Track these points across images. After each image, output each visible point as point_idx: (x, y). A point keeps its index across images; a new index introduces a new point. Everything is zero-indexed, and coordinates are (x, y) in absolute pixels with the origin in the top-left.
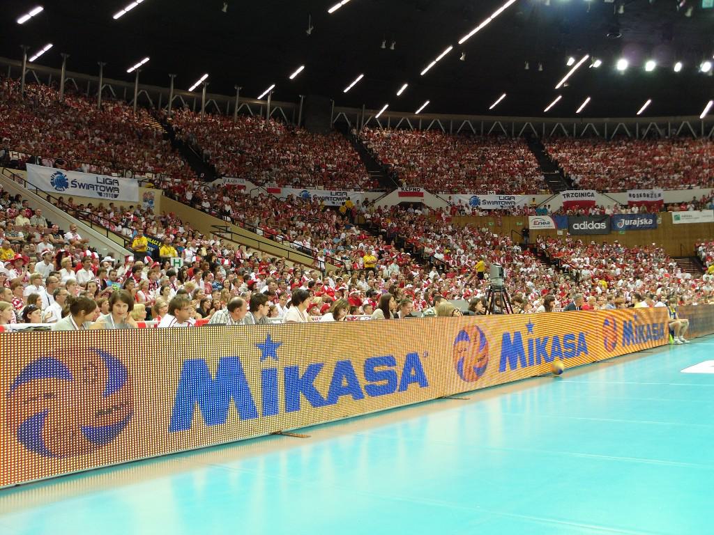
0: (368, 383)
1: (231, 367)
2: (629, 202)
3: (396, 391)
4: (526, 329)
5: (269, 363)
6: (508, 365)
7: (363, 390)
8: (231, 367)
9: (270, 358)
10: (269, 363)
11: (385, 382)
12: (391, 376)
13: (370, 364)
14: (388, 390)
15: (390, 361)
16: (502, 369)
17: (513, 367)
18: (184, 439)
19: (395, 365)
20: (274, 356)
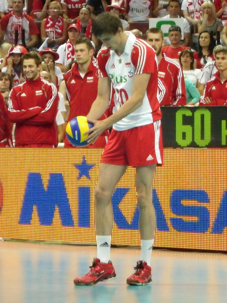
0: (174, 216)
1: (57, 180)
2: (145, 71)
3: (208, 233)
4: (76, 172)
5: (84, 182)
6: (35, 215)
7: (169, 223)
8: (57, 180)
9: (84, 177)
10: (84, 182)
11: (195, 219)
12: (203, 213)
13: (177, 197)
14: (200, 227)
15: (202, 196)
16: (25, 218)
17: (46, 219)
18: (25, 230)
19: (208, 201)
20: (88, 177)
